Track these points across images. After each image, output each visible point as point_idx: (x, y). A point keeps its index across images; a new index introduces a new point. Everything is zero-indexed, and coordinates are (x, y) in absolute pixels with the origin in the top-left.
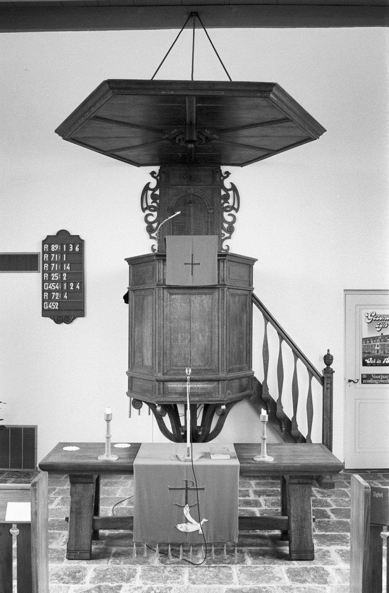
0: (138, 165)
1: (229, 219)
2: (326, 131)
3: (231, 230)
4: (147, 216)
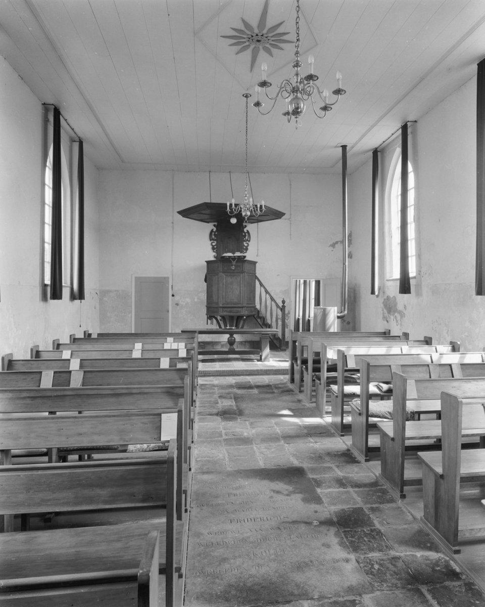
0: (208, 222)
1: (246, 245)
2: (256, 262)
3: (247, 249)
4: (212, 243)
